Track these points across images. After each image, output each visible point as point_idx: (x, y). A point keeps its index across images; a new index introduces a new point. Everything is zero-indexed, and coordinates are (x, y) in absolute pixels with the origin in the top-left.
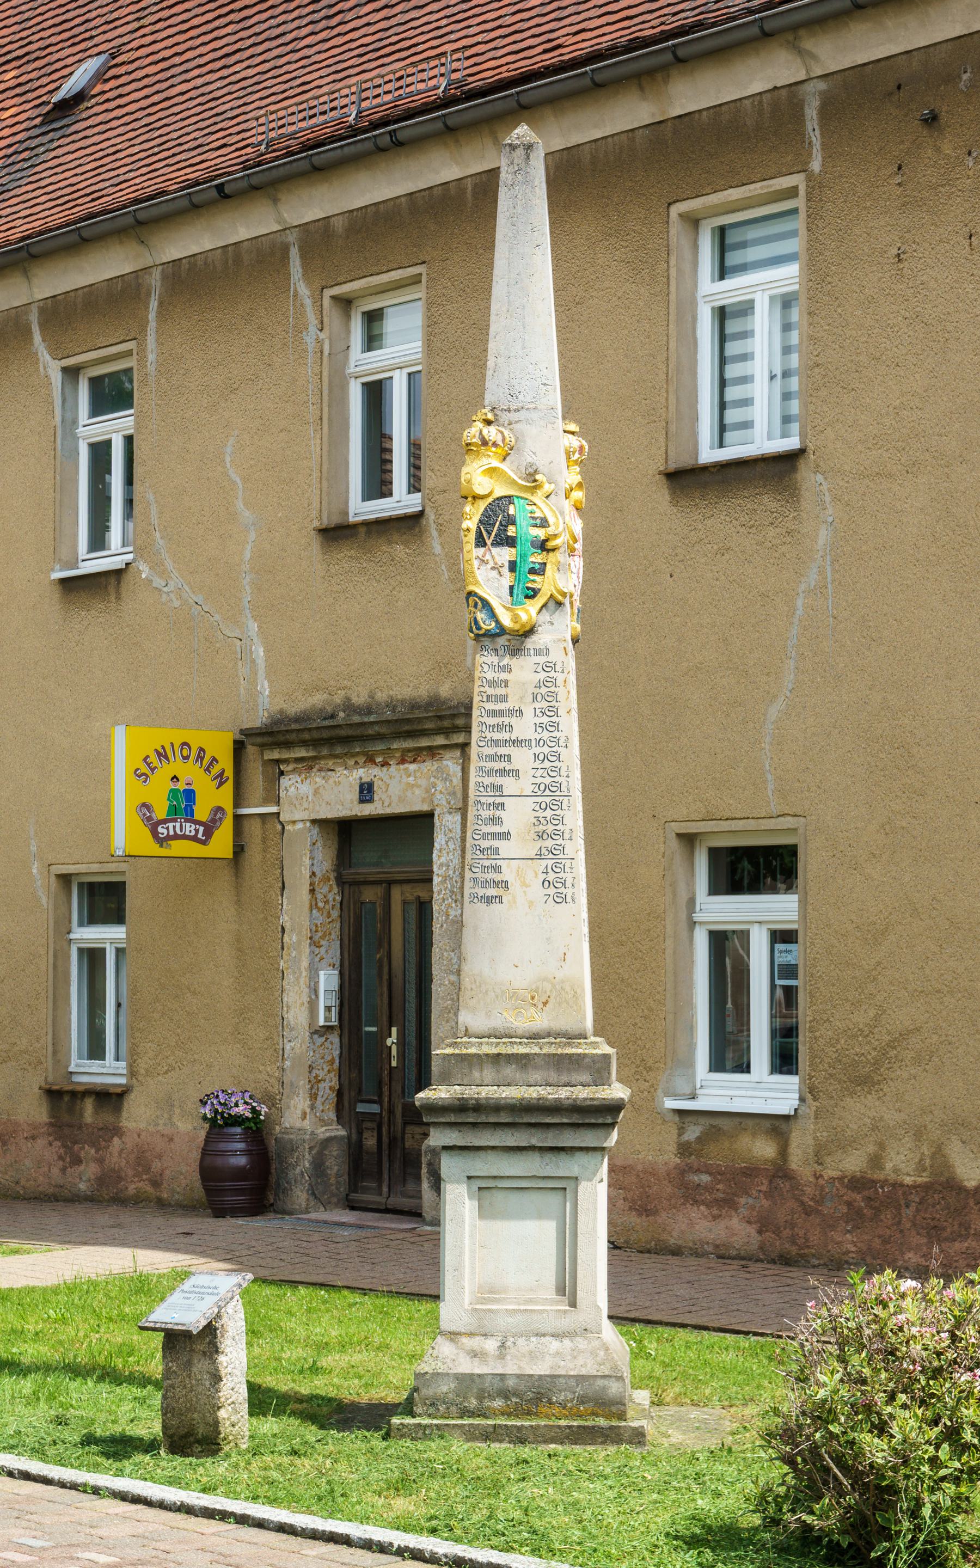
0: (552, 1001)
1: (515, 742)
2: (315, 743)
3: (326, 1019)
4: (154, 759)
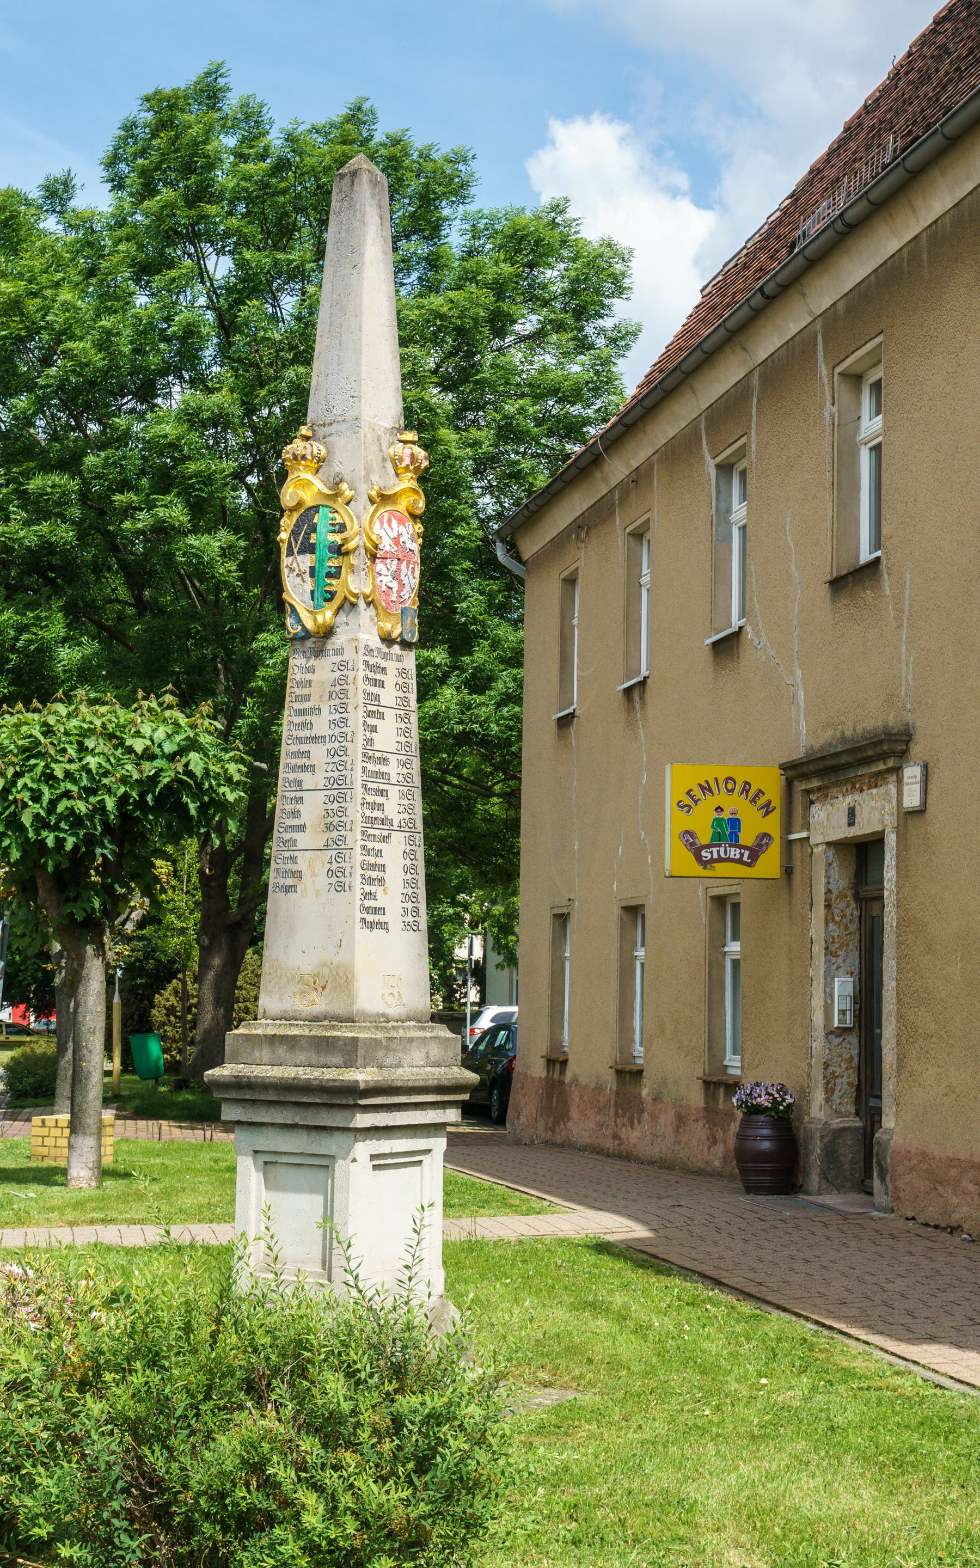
0: (329, 985)
1: (314, 739)
2: (820, 773)
3: (840, 1021)
4: (698, 793)
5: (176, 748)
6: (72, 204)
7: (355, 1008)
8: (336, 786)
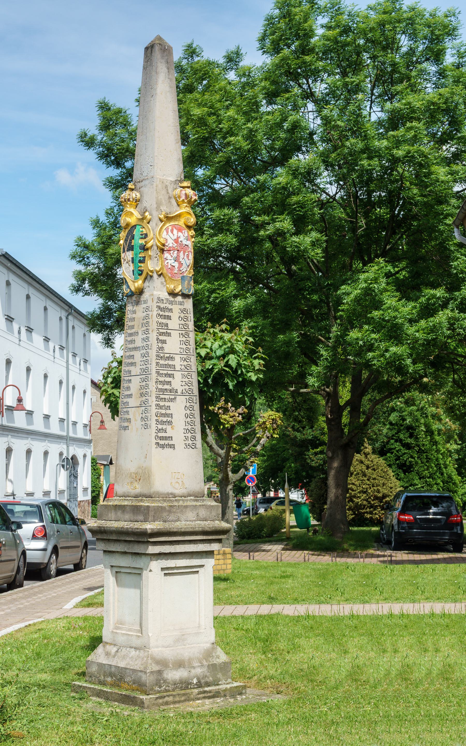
0: (142, 478)
1: (136, 349)
5: (222, 352)
6: (241, 64)
7: (152, 491)
8: (144, 373)
